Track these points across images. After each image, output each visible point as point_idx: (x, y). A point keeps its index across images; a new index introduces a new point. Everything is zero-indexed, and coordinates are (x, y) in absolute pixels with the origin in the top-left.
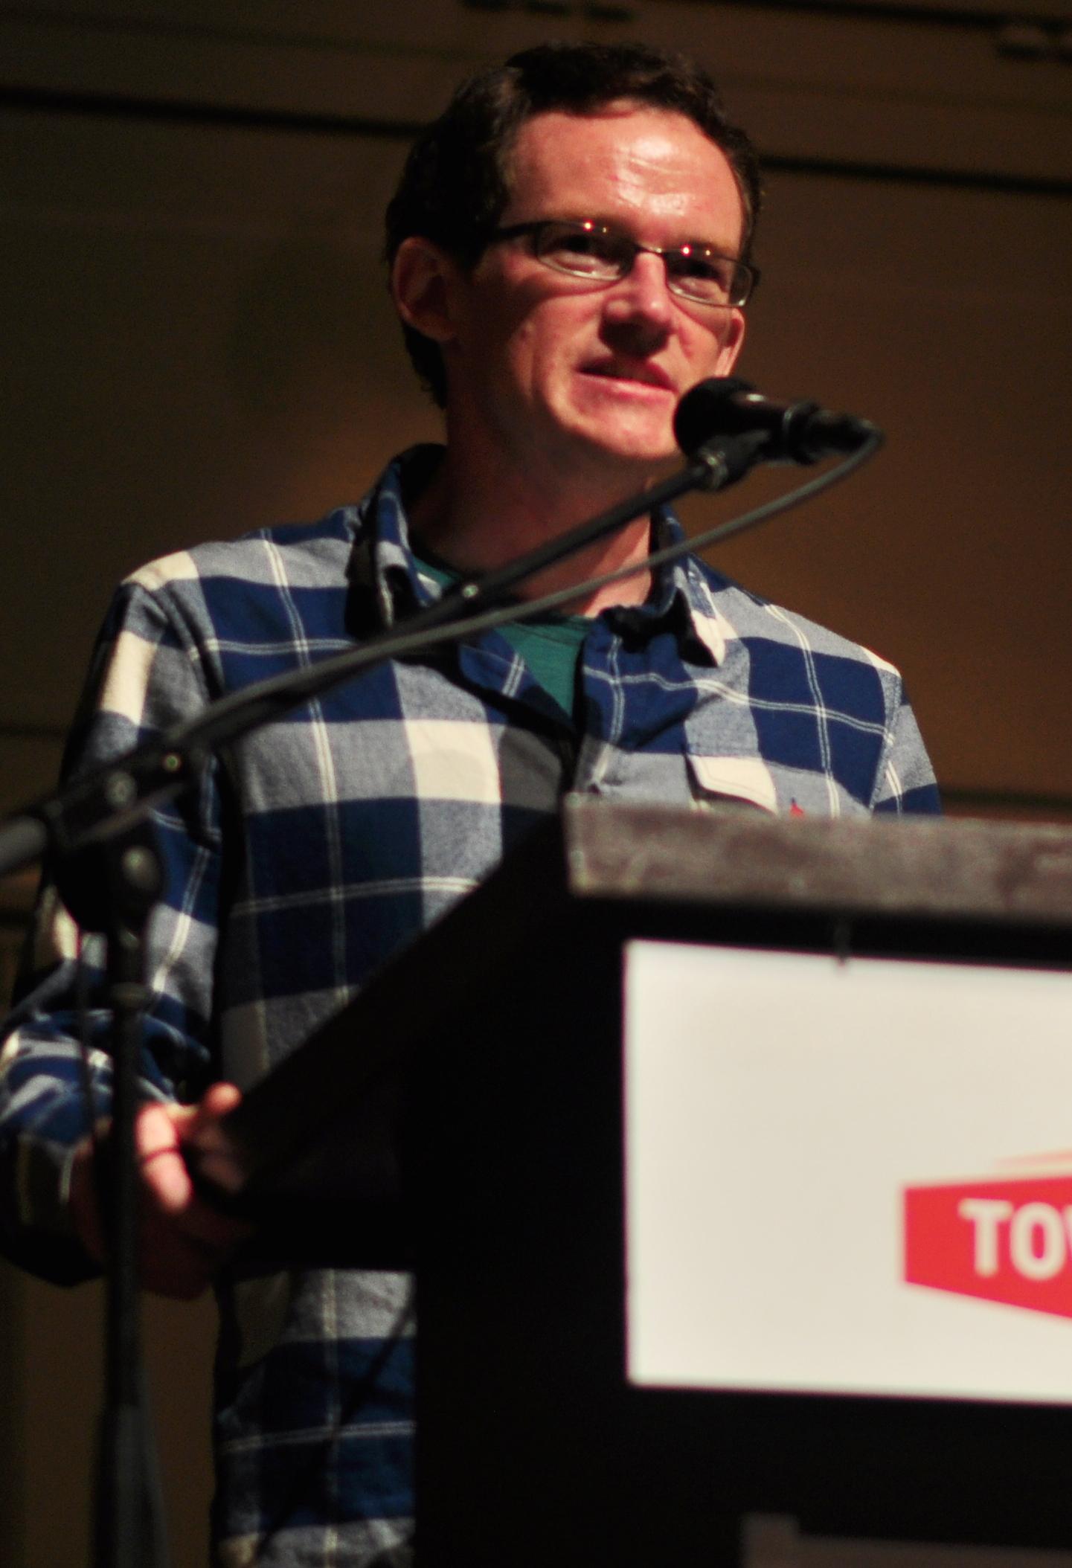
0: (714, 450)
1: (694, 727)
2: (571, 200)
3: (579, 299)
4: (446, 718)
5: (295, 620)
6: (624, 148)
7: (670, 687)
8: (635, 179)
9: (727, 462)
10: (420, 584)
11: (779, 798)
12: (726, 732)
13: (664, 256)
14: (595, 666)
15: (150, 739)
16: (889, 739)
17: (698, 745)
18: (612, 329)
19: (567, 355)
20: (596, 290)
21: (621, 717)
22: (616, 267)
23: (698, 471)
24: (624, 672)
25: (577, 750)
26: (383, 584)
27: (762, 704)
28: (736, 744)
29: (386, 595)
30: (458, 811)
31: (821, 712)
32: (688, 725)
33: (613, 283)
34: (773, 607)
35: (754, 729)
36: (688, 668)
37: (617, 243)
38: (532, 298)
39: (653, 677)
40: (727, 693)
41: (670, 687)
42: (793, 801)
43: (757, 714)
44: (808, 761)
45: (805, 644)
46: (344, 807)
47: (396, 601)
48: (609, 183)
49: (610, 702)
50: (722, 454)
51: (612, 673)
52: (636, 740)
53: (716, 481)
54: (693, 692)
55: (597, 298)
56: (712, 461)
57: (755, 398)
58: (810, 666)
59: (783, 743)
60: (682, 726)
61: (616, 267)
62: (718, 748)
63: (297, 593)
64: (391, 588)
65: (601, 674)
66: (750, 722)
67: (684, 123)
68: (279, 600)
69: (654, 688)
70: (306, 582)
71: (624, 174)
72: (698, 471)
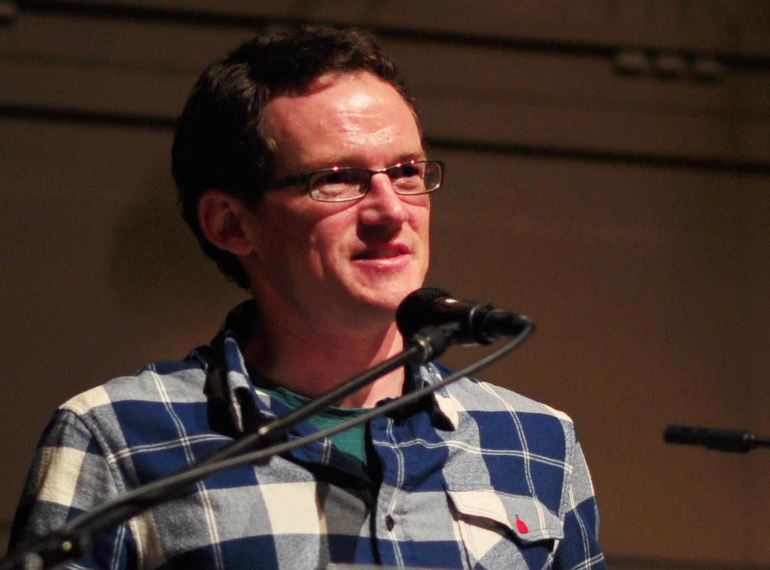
0: (424, 336)
1: (448, 472)
2: (321, 152)
3: (340, 210)
4: (286, 481)
5: (179, 424)
6: (341, 107)
7: (430, 446)
8: (357, 128)
9: (432, 343)
10: (257, 396)
11: (509, 516)
12: (470, 474)
13: (386, 172)
14: (380, 439)
16: (568, 468)
17: (453, 484)
18: (365, 229)
19: (341, 250)
20: (351, 206)
21: (403, 469)
22: (358, 187)
24: (399, 440)
25: (375, 494)
26: (234, 399)
27: (491, 452)
28: (477, 482)
29: (237, 407)
30: (299, 540)
31: (526, 455)
32: (445, 471)
33: (360, 199)
34: (484, 383)
35: (487, 470)
36: (439, 433)
37: (356, 172)
38: (317, 216)
39: (419, 441)
40: (465, 447)
41: (430, 446)
42: (517, 516)
43: (486, 458)
44: (522, 491)
45: (510, 408)
46: (223, 544)
47: (243, 410)
48: (340, 135)
49: (395, 460)
51: (392, 442)
52: (413, 484)
54: (445, 449)
55: (353, 210)
56: (422, 343)
57: (450, 301)
58: (517, 421)
59: (506, 478)
60: (441, 472)
61: (358, 187)
62: (466, 485)
63: (177, 406)
64: (239, 402)
65: (386, 444)
66: (484, 465)
67: (368, 77)
68: (167, 413)
69: (421, 448)
70: (183, 400)
71: (348, 126)
72: (414, 350)
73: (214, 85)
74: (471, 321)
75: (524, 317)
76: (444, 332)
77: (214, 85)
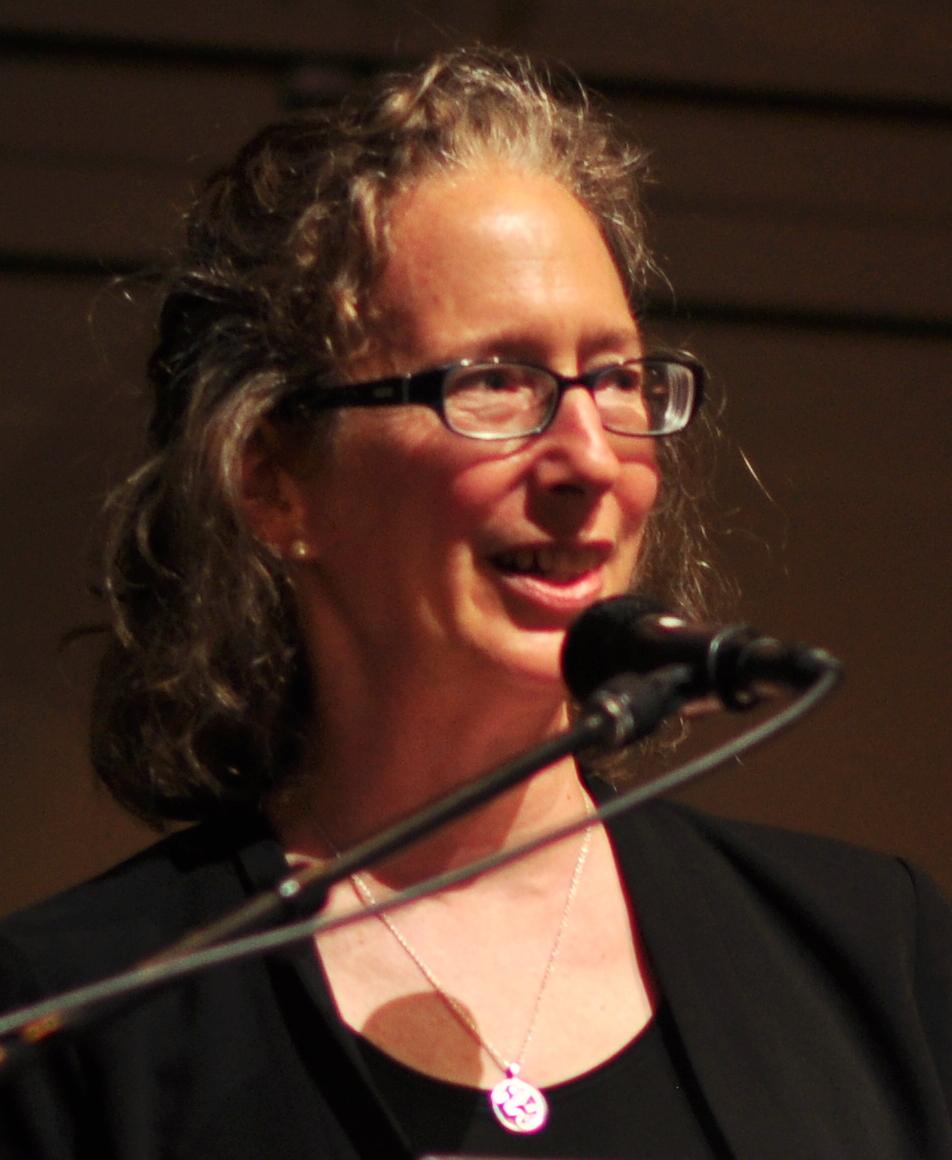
0: (616, 693)
9: (633, 709)
15: (252, 365)
23: (594, 722)
50: (625, 699)
53: (621, 730)
56: (613, 707)
57: (669, 622)
72: (594, 722)
73: (445, 153)
74: (711, 662)
75: (820, 654)
76: (657, 685)
77: (445, 153)
